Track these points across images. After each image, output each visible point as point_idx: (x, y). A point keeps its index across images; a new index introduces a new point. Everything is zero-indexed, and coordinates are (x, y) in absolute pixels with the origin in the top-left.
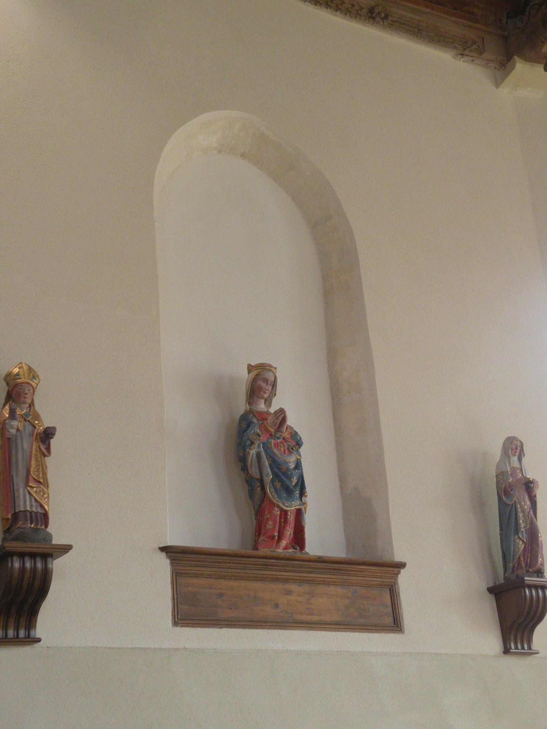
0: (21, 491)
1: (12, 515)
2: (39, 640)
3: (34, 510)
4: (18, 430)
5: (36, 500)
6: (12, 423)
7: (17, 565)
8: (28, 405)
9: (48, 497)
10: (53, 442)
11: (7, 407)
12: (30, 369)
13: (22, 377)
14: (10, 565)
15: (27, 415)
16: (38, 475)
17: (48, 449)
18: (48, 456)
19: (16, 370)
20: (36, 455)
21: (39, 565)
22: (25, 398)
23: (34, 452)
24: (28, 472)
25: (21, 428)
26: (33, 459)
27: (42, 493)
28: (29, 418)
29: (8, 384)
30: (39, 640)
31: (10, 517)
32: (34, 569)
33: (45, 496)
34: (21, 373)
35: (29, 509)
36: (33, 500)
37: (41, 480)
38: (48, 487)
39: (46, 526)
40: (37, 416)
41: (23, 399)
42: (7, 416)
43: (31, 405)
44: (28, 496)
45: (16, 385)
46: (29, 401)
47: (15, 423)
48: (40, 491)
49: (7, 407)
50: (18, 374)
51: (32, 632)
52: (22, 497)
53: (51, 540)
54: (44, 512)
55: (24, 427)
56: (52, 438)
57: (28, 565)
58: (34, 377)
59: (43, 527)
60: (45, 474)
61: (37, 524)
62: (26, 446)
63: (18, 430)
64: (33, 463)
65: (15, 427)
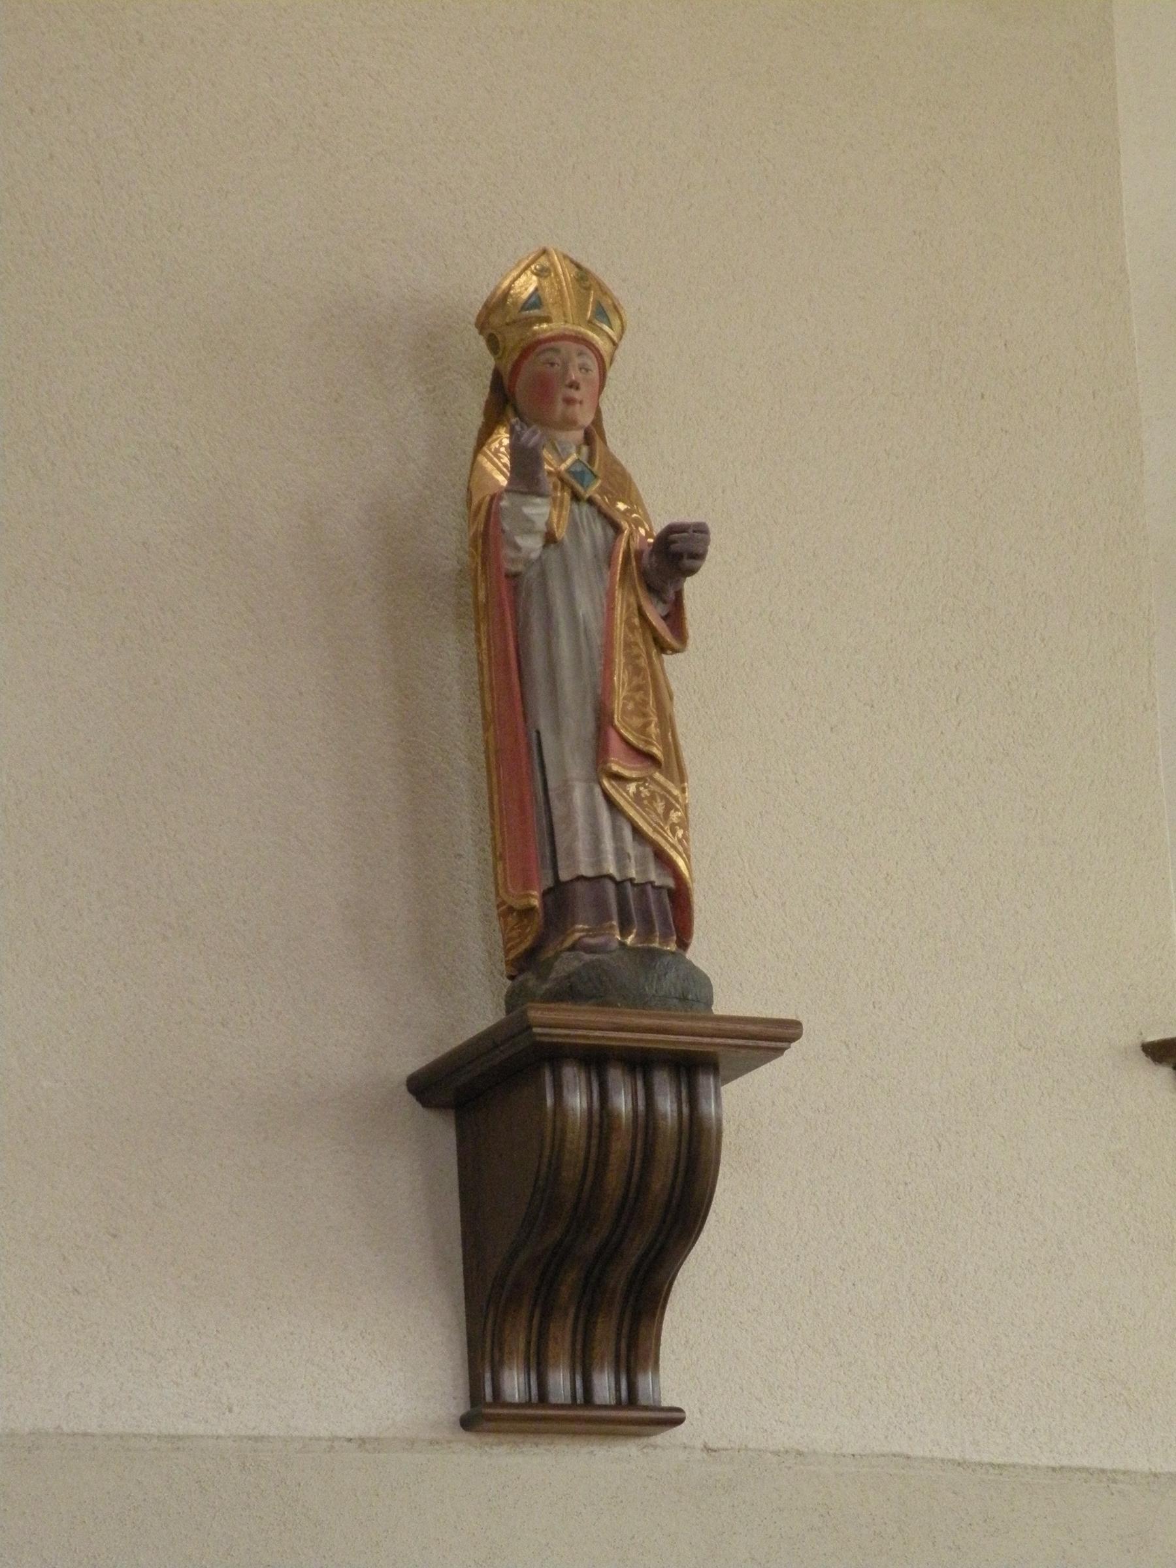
0: (578, 795)
1: (545, 894)
2: (672, 1419)
3: (633, 873)
4: (550, 539)
5: (637, 831)
6: (527, 510)
7: (577, 1101)
8: (579, 435)
9: (684, 823)
10: (690, 586)
11: (502, 439)
12: (583, 277)
13: (554, 312)
14: (549, 1101)
15: (581, 474)
16: (643, 730)
17: (675, 617)
18: (675, 651)
19: (527, 285)
20: (628, 645)
21: (667, 1105)
22: (569, 401)
23: (620, 631)
24: (603, 718)
25: (561, 533)
26: (620, 659)
27: (660, 806)
28: (593, 490)
29: (493, 344)
30: (672, 1419)
31: (536, 902)
32: (648, 1119)
33: (675, 816)
34: (548, 295)
35: (611, 868)
36: (627, 833)
37: (656, 751)
38: (682, 778)
39: (684, 934)
40: (621, 484)
41: (560, 407)
42: (503, 481)
43: (592, 436)
44: (605, 815)
45: (531, 348)
46: (586, 419)
47: (539, 511)
48: (652, 798)
49: (502, 439)
50: (536, 301)
51: (645, 1383)
52: (581, 821)
53: (709, 1003)
54: (670, 883)
55: (574, 526)
56: (692, 571)
57: (622, 1103)
58: (601, 313)
59: (672, 947)
60: (666, 722)
61: (647, 932)
62: (585, 606)
63: (550, 539)
64: (621, 676)
65: (541, 525)
